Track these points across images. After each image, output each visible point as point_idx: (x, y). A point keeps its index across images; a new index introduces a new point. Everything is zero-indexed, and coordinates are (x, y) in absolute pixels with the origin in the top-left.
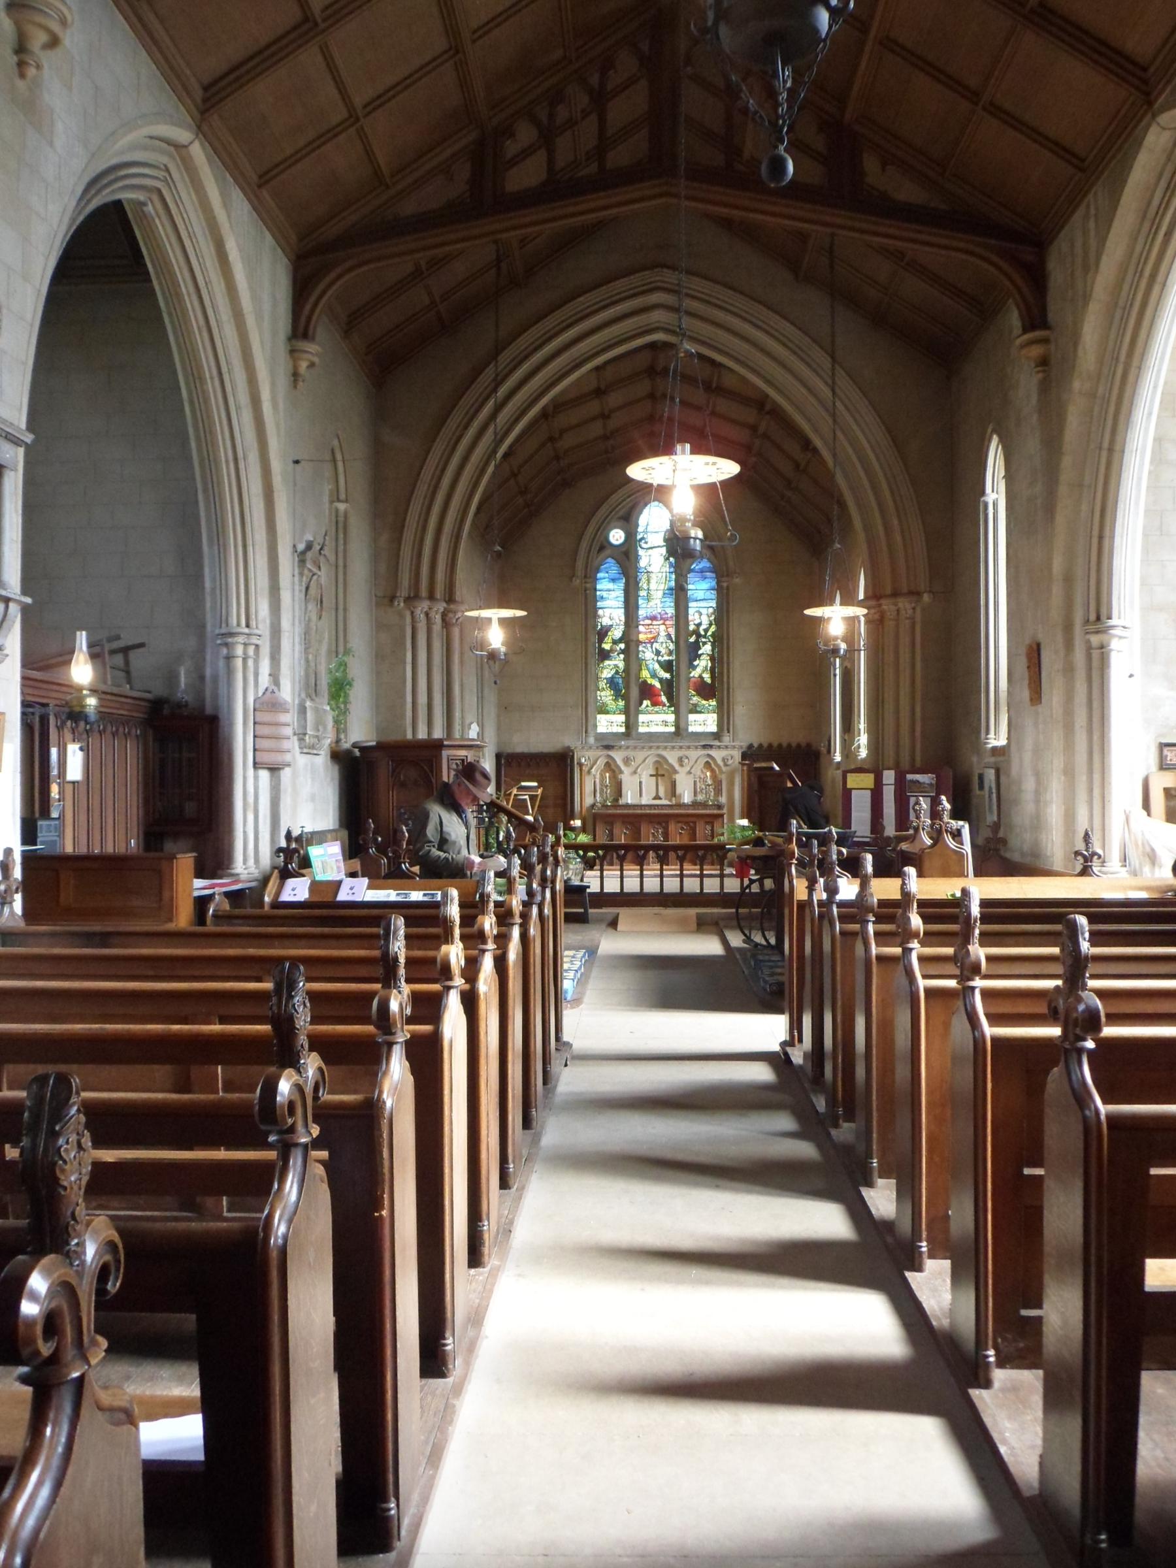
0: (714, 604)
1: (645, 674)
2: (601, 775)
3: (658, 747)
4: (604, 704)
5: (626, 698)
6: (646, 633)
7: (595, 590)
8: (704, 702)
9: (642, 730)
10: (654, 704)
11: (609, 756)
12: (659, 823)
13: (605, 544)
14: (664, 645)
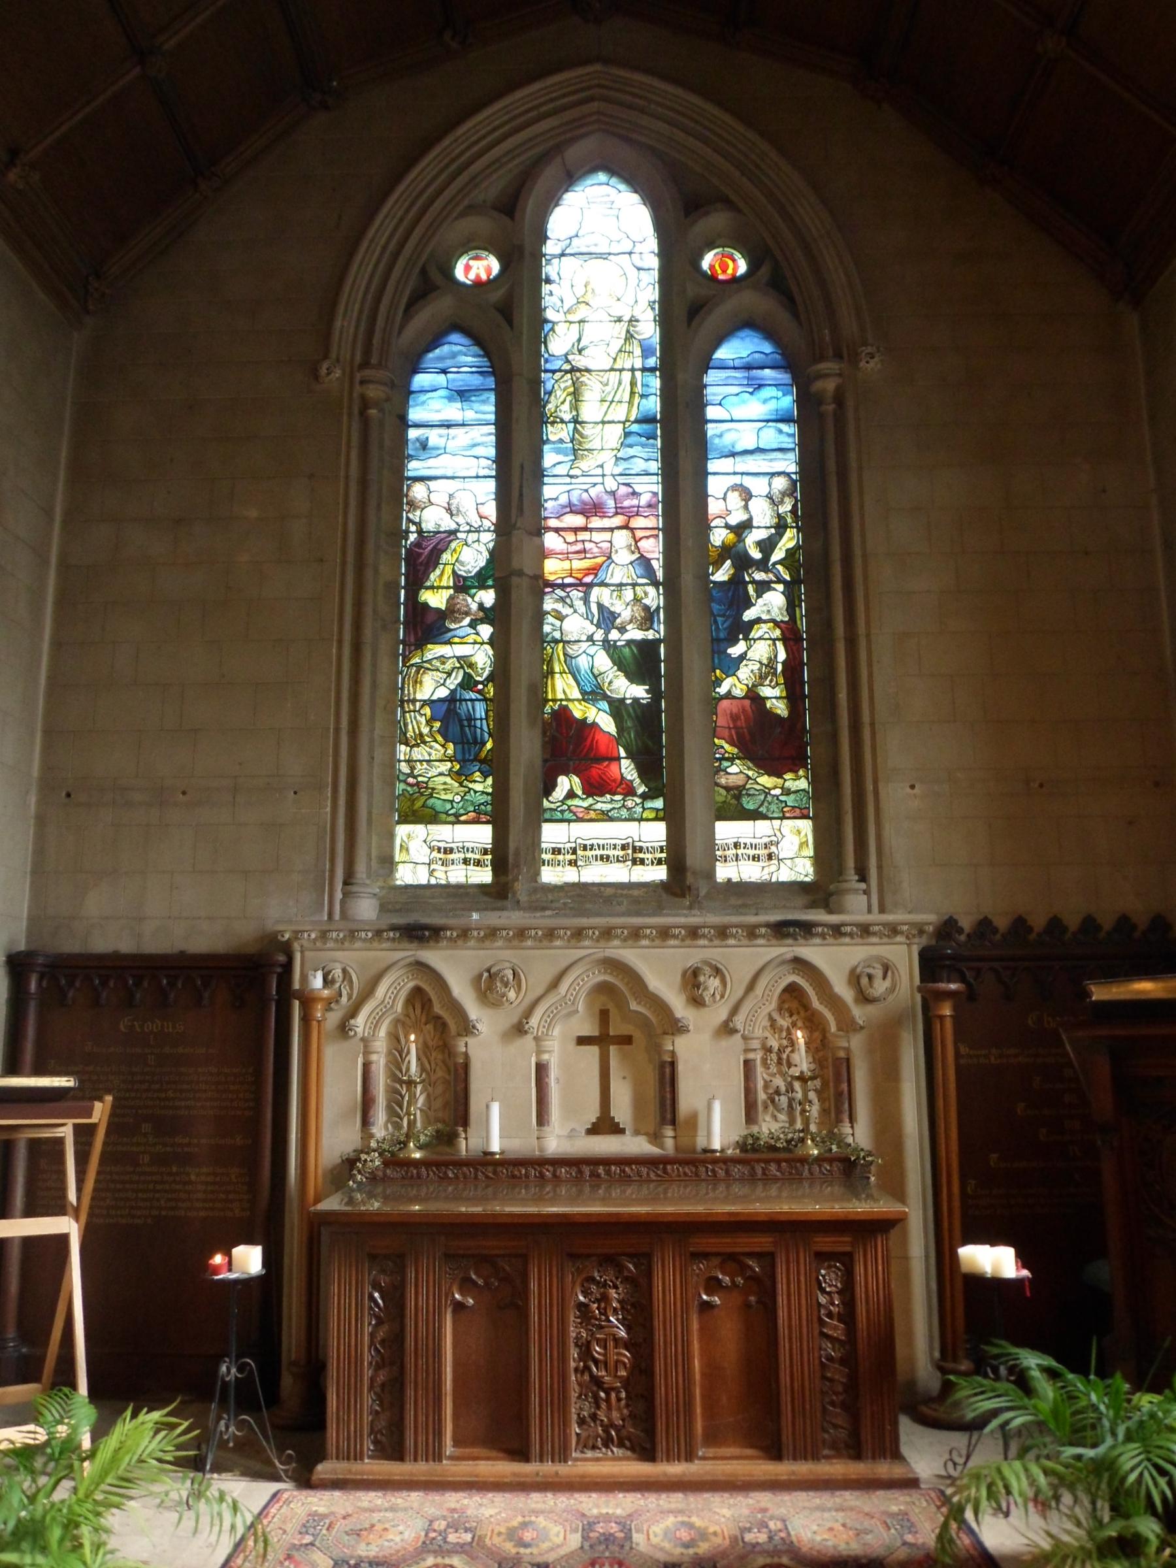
0: (789, 464)
1: (563, 687)
2: (395, 1038)
3: (607, 934)
4: (424, 789)
5: (496, 766)
6: (566, 556)
7: (403, 423)
8: (766, 781)
9: (549, 875)
10: (594, 788)
11: (421, 967)
12: (609, 1260)
13: (435, 276)
14: (628, 594)
